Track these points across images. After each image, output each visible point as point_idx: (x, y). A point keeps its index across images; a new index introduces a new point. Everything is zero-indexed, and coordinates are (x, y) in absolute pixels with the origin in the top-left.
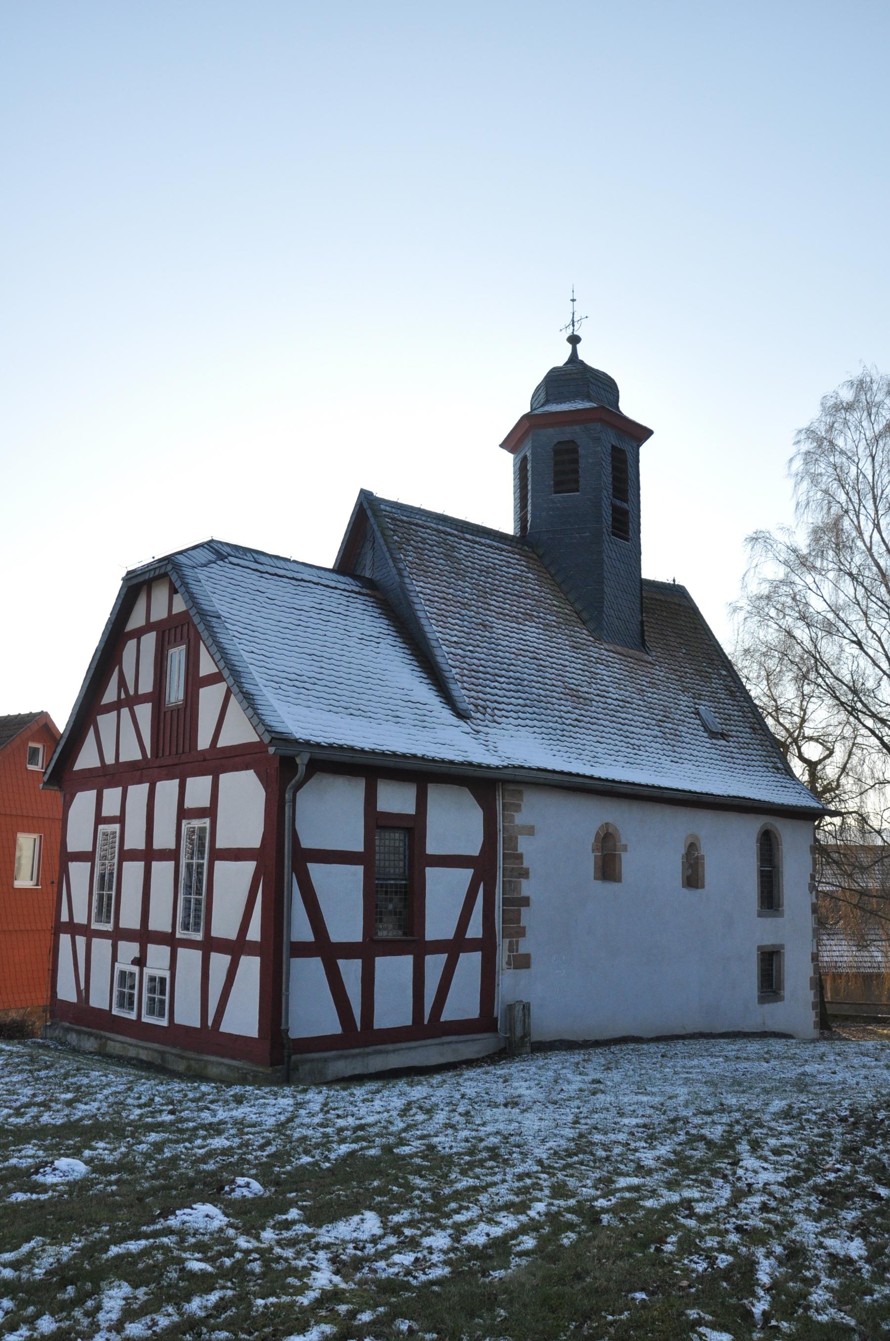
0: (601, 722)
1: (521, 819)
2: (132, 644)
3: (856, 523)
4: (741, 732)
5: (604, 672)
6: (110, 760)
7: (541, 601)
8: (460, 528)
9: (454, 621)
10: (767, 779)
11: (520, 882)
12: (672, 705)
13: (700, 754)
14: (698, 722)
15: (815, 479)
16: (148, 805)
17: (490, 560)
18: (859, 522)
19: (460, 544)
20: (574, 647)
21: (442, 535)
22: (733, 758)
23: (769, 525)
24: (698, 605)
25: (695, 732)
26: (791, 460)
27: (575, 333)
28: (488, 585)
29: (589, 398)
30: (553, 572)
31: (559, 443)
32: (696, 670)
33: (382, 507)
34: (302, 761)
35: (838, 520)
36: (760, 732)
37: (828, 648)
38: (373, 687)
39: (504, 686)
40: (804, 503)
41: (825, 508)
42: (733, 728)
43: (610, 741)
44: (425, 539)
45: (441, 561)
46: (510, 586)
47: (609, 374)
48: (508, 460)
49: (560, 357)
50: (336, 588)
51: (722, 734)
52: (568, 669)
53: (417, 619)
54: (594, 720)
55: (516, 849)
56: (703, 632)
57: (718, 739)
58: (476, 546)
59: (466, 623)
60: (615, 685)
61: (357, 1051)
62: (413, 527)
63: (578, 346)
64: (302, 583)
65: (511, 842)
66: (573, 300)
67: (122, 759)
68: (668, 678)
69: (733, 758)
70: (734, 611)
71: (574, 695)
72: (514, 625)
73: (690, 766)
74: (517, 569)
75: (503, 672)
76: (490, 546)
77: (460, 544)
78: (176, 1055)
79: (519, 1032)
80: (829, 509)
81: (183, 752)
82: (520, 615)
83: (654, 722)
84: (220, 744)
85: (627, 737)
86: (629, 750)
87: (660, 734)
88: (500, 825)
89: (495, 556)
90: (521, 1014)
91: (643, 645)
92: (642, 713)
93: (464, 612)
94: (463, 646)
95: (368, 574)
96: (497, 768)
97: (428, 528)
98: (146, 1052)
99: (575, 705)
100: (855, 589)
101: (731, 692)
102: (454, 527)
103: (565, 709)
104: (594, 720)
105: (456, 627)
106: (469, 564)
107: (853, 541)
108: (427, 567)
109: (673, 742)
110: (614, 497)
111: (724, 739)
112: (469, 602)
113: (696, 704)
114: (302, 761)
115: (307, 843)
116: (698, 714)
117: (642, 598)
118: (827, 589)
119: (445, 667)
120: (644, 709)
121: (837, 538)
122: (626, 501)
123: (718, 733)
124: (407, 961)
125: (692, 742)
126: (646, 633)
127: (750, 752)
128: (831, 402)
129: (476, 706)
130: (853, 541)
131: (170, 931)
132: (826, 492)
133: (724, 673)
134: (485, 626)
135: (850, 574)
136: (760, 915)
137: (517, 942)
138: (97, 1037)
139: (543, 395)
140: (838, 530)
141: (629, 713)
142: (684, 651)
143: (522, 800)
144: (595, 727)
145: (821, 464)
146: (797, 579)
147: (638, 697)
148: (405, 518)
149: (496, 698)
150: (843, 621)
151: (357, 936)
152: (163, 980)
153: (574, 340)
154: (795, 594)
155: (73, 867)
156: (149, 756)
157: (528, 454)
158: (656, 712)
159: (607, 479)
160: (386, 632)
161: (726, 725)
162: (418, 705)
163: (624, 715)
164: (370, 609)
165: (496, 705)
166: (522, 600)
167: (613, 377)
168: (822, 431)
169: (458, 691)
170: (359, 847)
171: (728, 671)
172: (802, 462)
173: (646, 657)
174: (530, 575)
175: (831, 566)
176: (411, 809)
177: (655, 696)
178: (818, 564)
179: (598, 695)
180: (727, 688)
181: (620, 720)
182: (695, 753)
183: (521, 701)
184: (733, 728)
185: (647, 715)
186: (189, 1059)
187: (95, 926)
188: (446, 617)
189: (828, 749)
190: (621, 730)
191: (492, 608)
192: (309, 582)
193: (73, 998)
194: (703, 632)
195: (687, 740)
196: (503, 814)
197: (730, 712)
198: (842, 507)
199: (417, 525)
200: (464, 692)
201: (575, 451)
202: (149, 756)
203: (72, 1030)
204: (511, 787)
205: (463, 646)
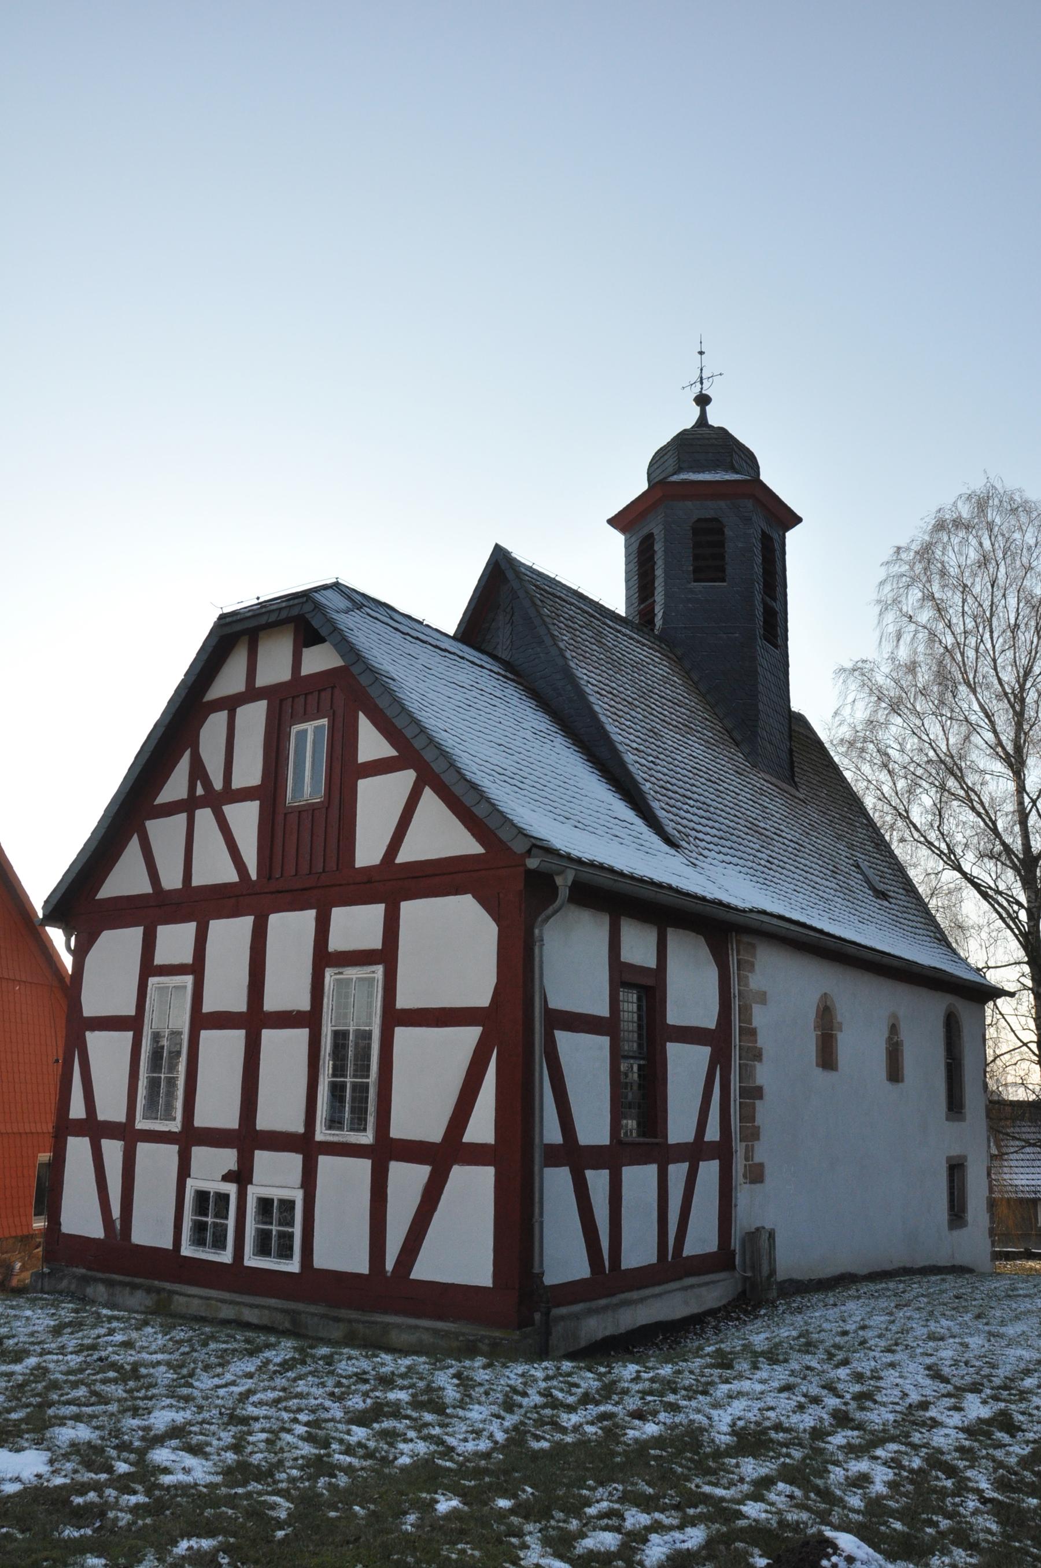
1: (756, 981)
2: (217, 721)
6: (171, 879)
7: (693, 712)
11: (755, 1066)
16: (252, 948)
20: (736, 772)
27: (704, 392)
30: (696, 679)
31: (699, 520)
33: (523, 570)
34: (564, 882)
45: (594, 647)
48: (617, 540)
49: (687, 418)
61: (603, 1302)
63: (708, 408)
64: (447, 654)
65: (746, 1012)
66: (701, 353)
67: (196, 882)
71: (754, 829)
78: (323, 1316)
79: (765, 1270)
84: (403, 856)
88: (735, 989)
90: (766, 1245)
93: (633, 713)
95: (504, 655)
97: (572, 604)
98: (256, 1311)
102: (594, 608)
111: (887, 900)
114: (564, 882)
116: (858, 867)
124: (652, 1169)
126: (796, 764)
129: (679, 832)
131: (301, 1130)
136: (947, 1119)
137: (753, 1146)
138: (149, 1290)
143: (754, 955)
151: (603, 1138)
152: (288, 1205)
153: (703, 400)
155: (94, 1039)
156: (254, 876)
157: (658, 532)
164: (524, 698)
170: (602, 1009)
173: (797, 794)
174: (675, 679)
176: (652, 964)
186: (350, 1321)
187: (141, 1124)
192: (454, 654)
193: (97, 1231)
196: (738, 975)
201: (721, 532)
202: (254, 876)
203: (96, 1280)
204: (746, 939)
205: (645, 756)
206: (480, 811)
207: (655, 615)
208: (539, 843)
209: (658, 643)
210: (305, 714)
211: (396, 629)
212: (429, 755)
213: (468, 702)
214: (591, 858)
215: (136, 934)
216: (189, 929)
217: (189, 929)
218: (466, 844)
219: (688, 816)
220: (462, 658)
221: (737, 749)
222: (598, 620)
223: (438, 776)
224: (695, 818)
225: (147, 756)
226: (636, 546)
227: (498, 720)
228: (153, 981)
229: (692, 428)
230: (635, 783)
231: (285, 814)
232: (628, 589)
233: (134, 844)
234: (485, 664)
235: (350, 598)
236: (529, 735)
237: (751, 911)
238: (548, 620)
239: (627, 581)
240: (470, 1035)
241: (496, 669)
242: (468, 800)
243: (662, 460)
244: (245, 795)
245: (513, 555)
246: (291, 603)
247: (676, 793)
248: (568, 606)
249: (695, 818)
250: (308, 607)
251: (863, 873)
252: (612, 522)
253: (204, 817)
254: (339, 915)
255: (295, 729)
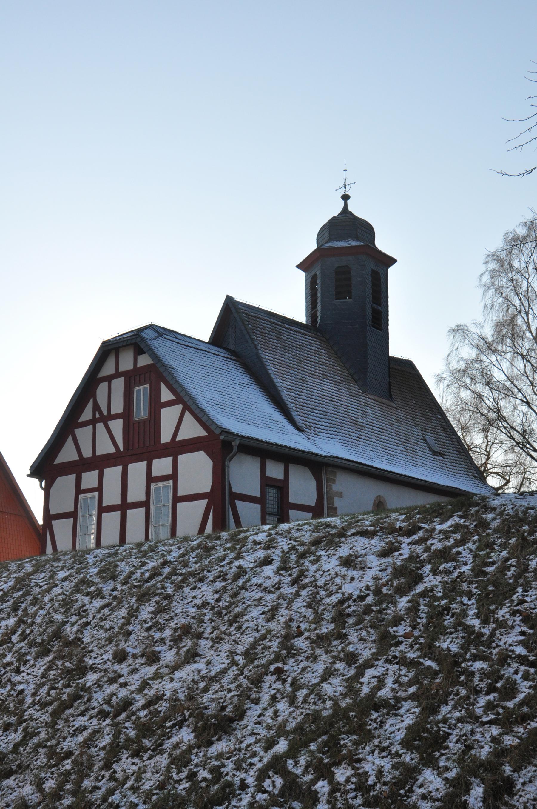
0: (371, 439)
1: (336, 487)
3: (526, 320)
4: (452, 453)
5: (370, 411)
6: (87, 453)
7: (331, 367)
8: (281, 321)
9: (287, 377)
10: (469, 481)
12: (409, 434)
13: (428, 463)
14: (425, 445)
15: (499, 291)
16: (122, 478)
17: (300, 341)
18: (528, 319)
19: (283, 330)
20: (351, 395)
21: (273, 325)
22: (447, 468)
23: (465, 320)
24: (421, 374)
25: (424, 450)
26: (482, 275)
27: (346, 193)
28: (301, 356)
29: (357, 238)
31: (339, 267)
32: (422, 414)
33: (240, 307)
35: (514, 318)
36: (463, 454)
37: (506, 406)
38: (254, 411)
39: (318, 415)
40: (490, 306)
41: (505, 309)
42: (446, 450)
43: (377, 450)
44: (265, 327)
45: (275, 341)
46: (313, 357)
47: (369, 222)
48: (302, 275)
49: (336, 209)
50: (219, 355)
51: (440, 453)
52: (350, 408)
53: (268, 375)
54: (367, 438)
55: (333, 504)
56: (425, 391)
57: (437, 456)
58: (292, 332)
59: (293, 378)
60: (377, 420)
62: (258, 319)
63: (348, 201)
64: (202, 352)
65: (331, 500)
66: (345, 170)
67: (98, 453)
68: (406, 418)
69: (447, 468)
70: (440, 381)
71: (355, 423)
72: (318, 381)
73: (423, 469)
74: (316, 347)
75: (317, 408)
76: (299, 333)
77: (283, 330)
80: (508, 310)
81: (149, 445)
82: (320, 375)
83: (400, 443)
84: (179, 438)
85: (386, 449)
86: (388, 457)
87: (404, 450)
88: (325, 490)
89: (302, 338)
91: (390, 397)
92: (393, 437)
93: (292, 372)
94: (294, 392)
95: (232, 347)
96: (325, 456)
97: (266, 320)
99: (356, 429)
100: (525, 366)
101: (444, 428)
102: (278, 320)
103: (352, 431)
104: (367, 438)
105: (289, 380)
106: (290, 343)
107: (524, 332)
108: (269, 344)
109: (412, 455)
110: (373, 302)
111: (441, 456)
112: (293, 366)
113: (423, 434)
114: (235, 444)
115: (235, 490)
116: (425, 440)
117: (389, 368)
118: (505, 365)
119: (288, 403)
120: (394, 434)
121: (513, 330)
122: (380, 305)
123: (437, 452)
125: (423, 456)
127: (457, 465)
128: (511, 236)
129: (306, 425)
130: (524, 332)
132: (506, 298)
133: (439, 417)
134: (303, 380)
135: (522, 355)
139: (326, 235)
140: (513, 325)
141: (386, 436)
142: (414, 402)
144: (368, 442)
145: (503, 279)
146: (484, 358)
147: (390, 427)
148: (252, 314)
149: (315, 421)
150: (516, 387)
153: (346, 198)
154: (483, 369)
156: (122, 450)
157: (318, 273)
158: (401, 437)
159: (369, 291)
160: (250, 382)
161: (442, 448)
162: (277, 422)
163: (383, 437)
164: (238, 368)
165: (315, 425)
166: (321, 366)
167: (371, 223)
168: (503, 255)
169: (296, 416)
170: (258, 494)
171: (442, 416)
172: (489, 277)
173: (392, 404)
174: (323, 351)
175: (508, 349)
176: (281, 477)
177: (399, 427)
178: (499, 348)
179: (368, 424)
180: (442, 426)
181: (381, 440)
182: (425, 462)
183: (327, 424)
184: (446, 450)
185: (396, 438)
188: (283, 374)
189: (505, 479)
190: (382, 445)
191: (306, 370)
192: (205, 351)
194: (425, 391)
195: (420, 455)
197: (444, 441)
198: (517, 309)
199: (259, 318)
200: (299, 417)
202: (122, 450)
204: (330, 469)
205: (294, 392)
206: (204, 419)
207: (318, 317)
208: (224, 430)
209: (315, 333)
210: (140, 383)
211: (178, 343)
212: (186, 399)
213: (208, 374)
214: (248, 435)
215: (73, 477)
216: (96, 473)
217: (96, 473)
218: (201, 432)
219: (314, 418)
220: (209, 352)
221: (355, 384)
222: (280, 326)
223: (189, 407)
224: (317, 419)
225: (74, 401)
226: (310, 280)
227: (221, 380)
228: (81, 496)
229: (339, 214)
230: (285, 404)
231: (133, 424)
232: (307, 302)
233: (70, 440)
234: (220, 354)
235: (157, 332)
236: (236, 386)
237: (329, 457)
238: (250, 331)
239: (306, 298)
240: (204, 503)
241: (226, 355)
242: (200, 415)
243: (323, 233)
244: (117, 416)
245: (236, 299)
246: (132, 337)
247: (309, 407)
248: (263, 321)
249: (317, 419)
250: (139, 339)
251: (427, 443)
252: (298, 267)
253: (100, 426)
254: (155, 462)
255: (136, 389)
